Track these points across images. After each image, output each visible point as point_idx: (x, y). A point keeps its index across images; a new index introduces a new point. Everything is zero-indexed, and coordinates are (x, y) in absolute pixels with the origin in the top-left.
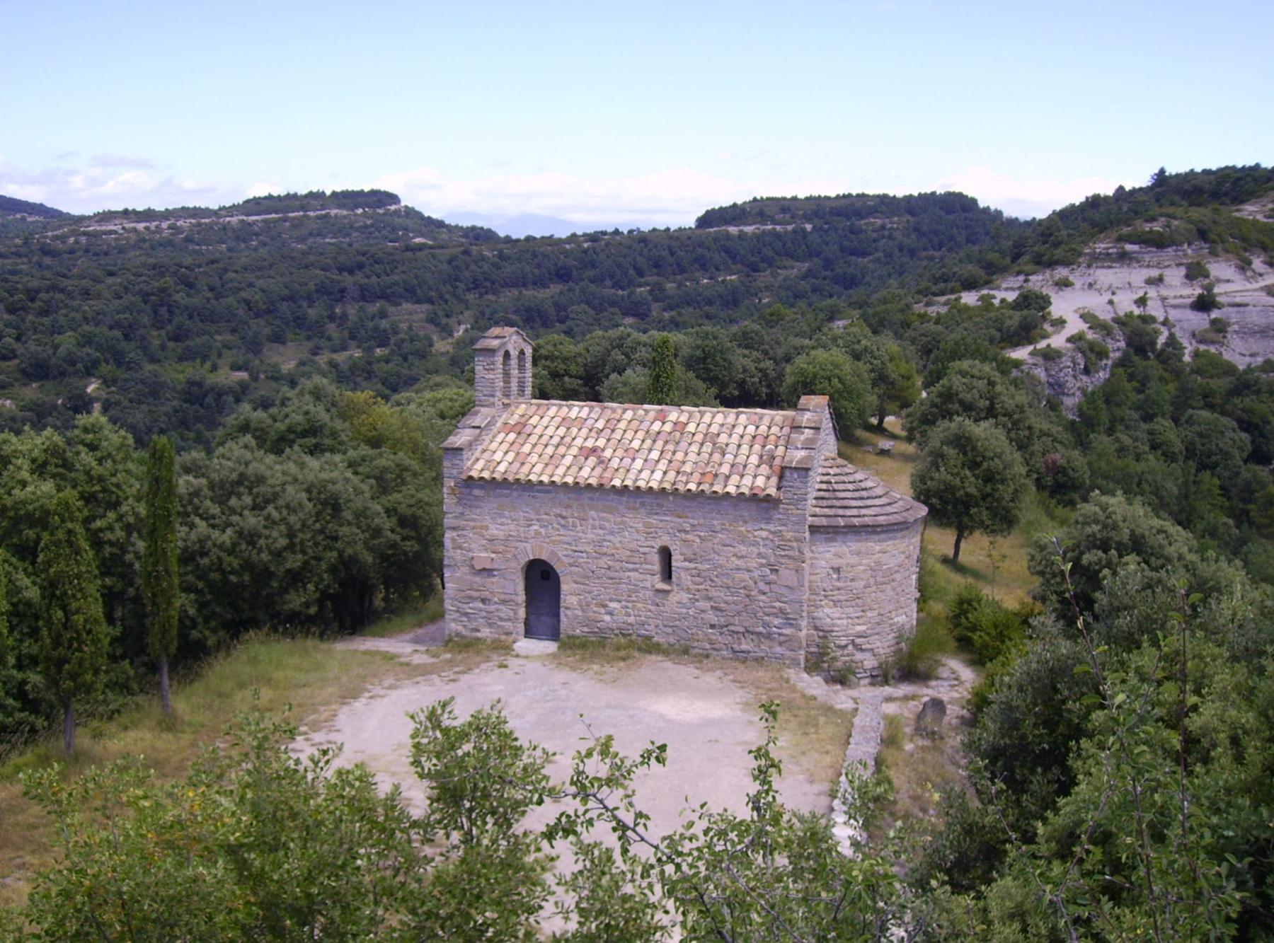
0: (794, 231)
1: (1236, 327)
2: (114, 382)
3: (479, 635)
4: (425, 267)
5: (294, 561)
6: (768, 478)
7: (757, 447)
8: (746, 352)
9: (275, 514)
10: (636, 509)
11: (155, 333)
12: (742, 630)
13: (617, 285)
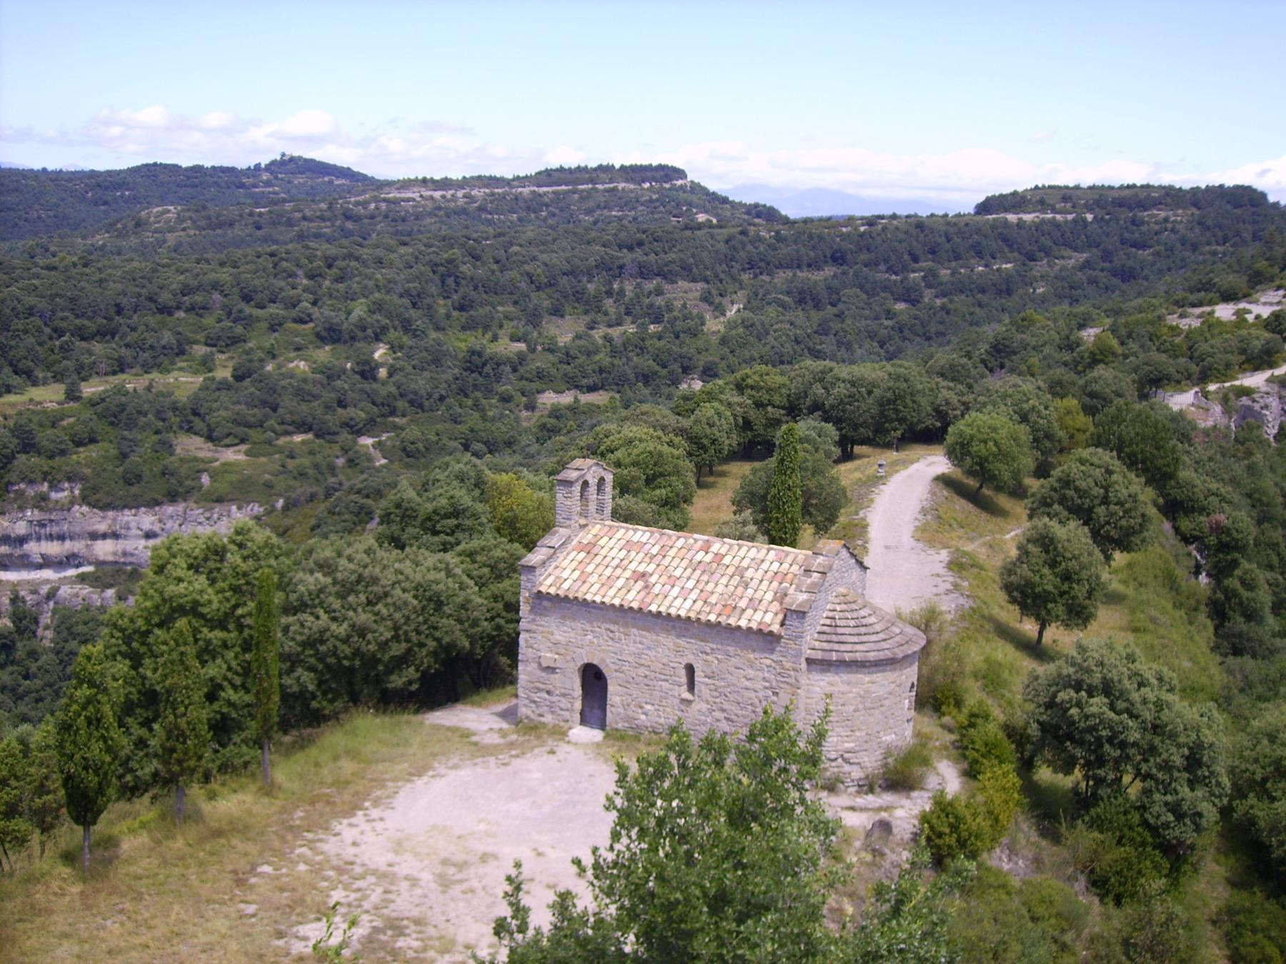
0: (1074, 221)
2: (401, 348)
3: (542, 719)
4: (702, 247)
5: (397, 649)
6: (776, 614)
7: (775, 584)
8: (951, 384)
9: (384, 612)
11: (442, 302)
13: (890, 270)
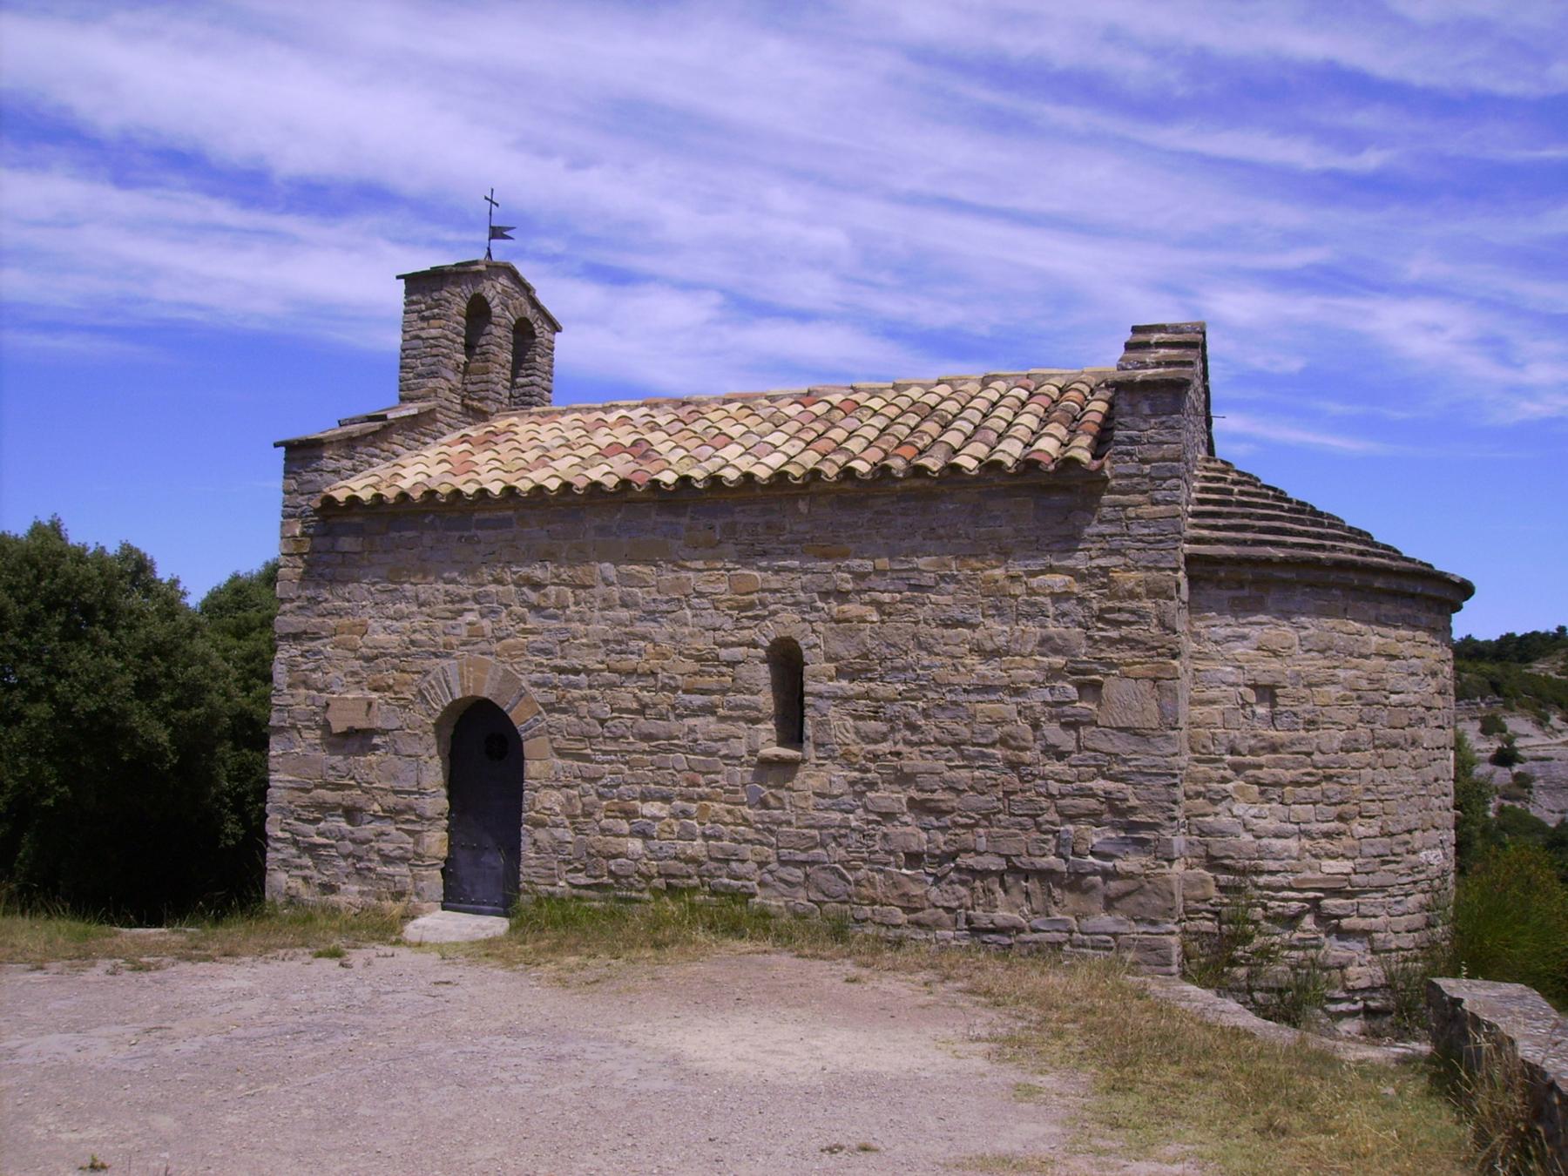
1: (1542, 782)
10: (713, 545)
12: (996, 864)
